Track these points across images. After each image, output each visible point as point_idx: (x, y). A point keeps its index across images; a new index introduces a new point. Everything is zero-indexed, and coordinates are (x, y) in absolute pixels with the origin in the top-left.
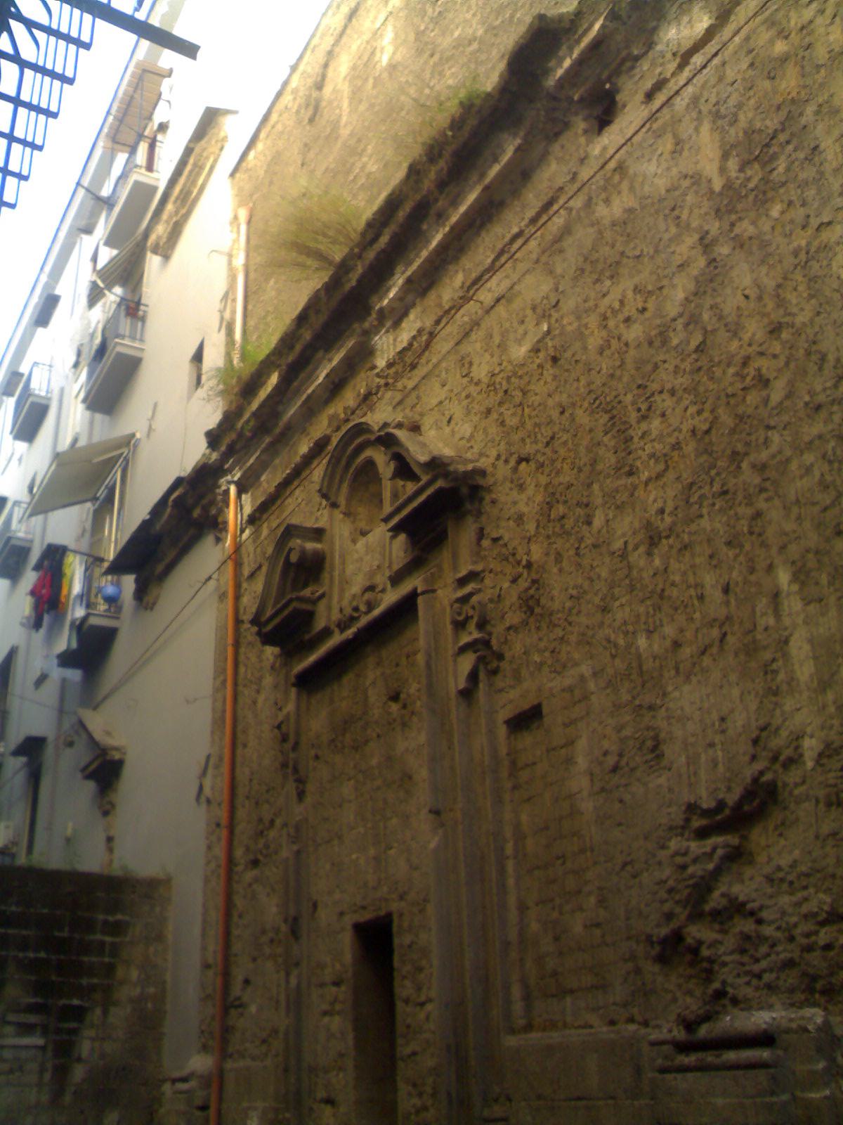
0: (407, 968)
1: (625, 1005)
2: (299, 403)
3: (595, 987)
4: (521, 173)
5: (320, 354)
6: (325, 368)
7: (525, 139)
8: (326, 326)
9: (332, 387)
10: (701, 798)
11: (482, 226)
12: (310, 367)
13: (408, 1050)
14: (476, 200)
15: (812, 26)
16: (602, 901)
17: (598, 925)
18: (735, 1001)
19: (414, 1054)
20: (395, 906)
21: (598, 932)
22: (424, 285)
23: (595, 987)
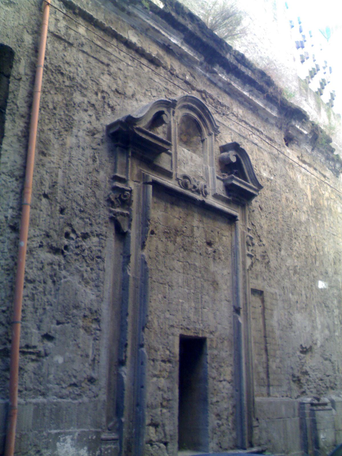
0: (215, 364)
1: (286, 392)
2: (152, 24)
3: (278, 386)
4: (266, 119)
5: (183, 36)
6: (178, 41)
7: (275, 117)
8: (198, 39)
9: (166, 44)
10: (316, 344)
11: (250, 109)
12: (171, 28)
13: (214, 400)
14: (260, 106)
15: (228, 120)
16: (281, 361)
17: (279, 368)
18: (307, 394)
19: (217, 402)
20: (207, 335)
21: (279, 370)
22: (227, 90)
23: (278, 386)
